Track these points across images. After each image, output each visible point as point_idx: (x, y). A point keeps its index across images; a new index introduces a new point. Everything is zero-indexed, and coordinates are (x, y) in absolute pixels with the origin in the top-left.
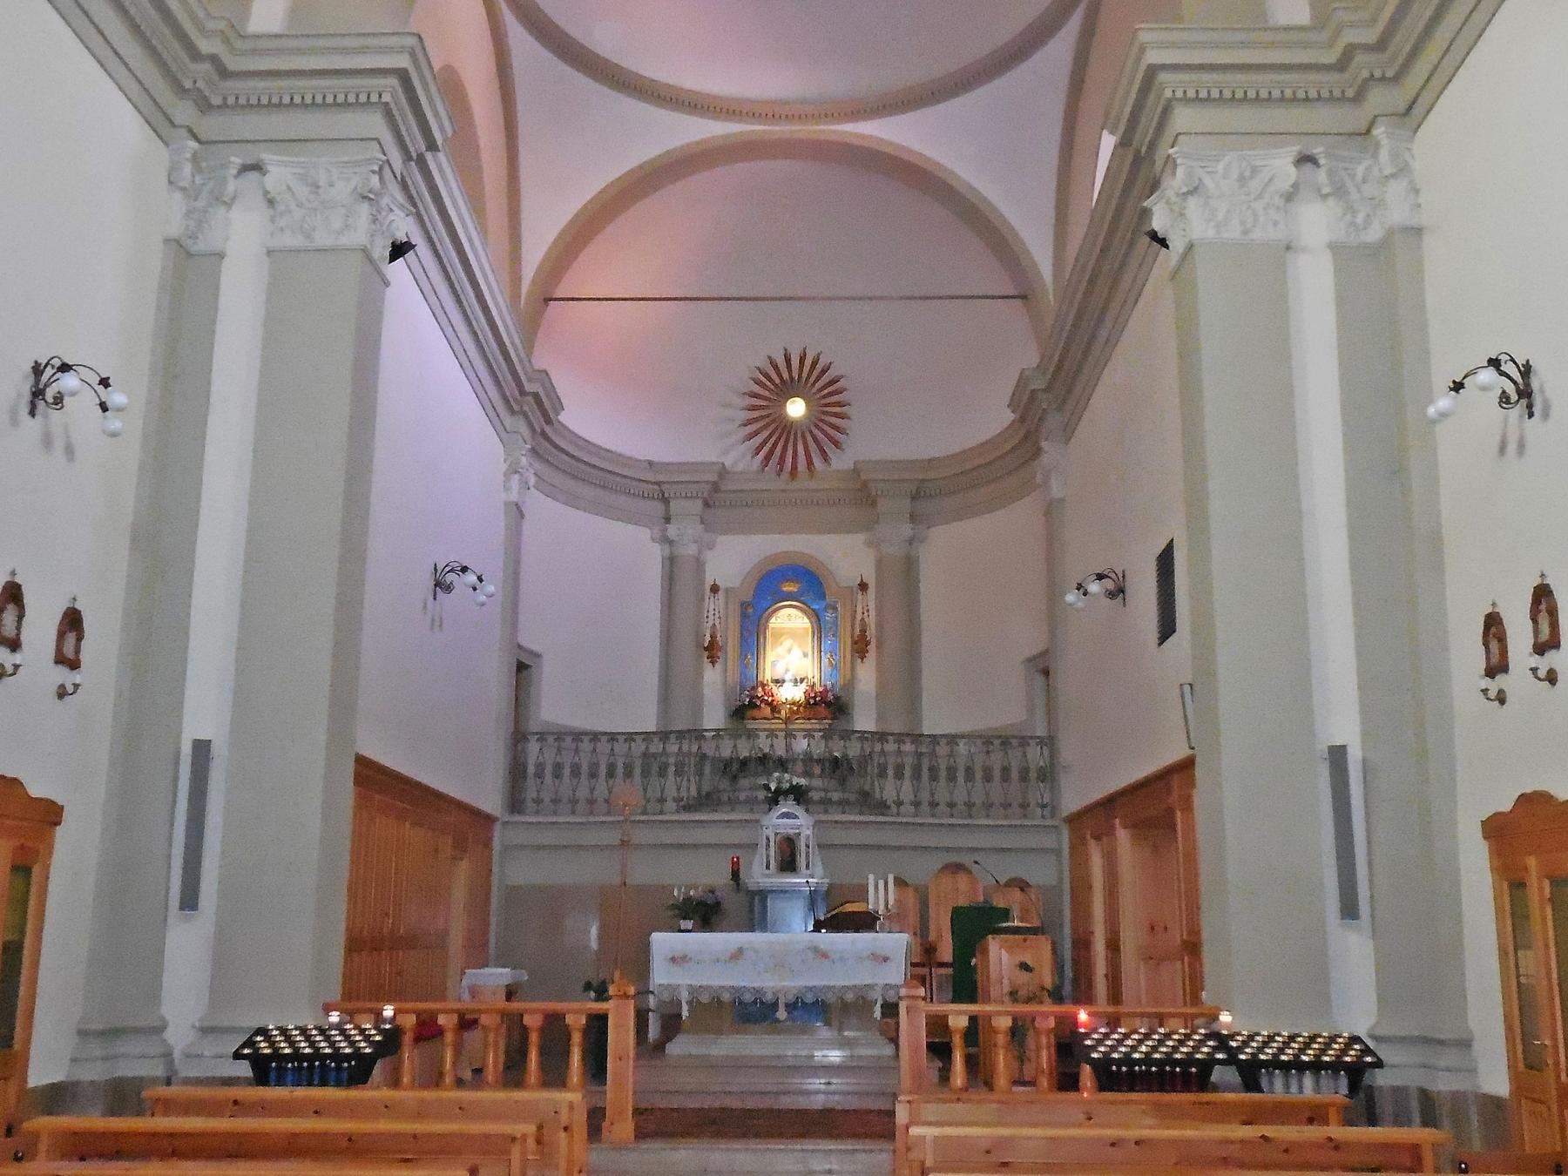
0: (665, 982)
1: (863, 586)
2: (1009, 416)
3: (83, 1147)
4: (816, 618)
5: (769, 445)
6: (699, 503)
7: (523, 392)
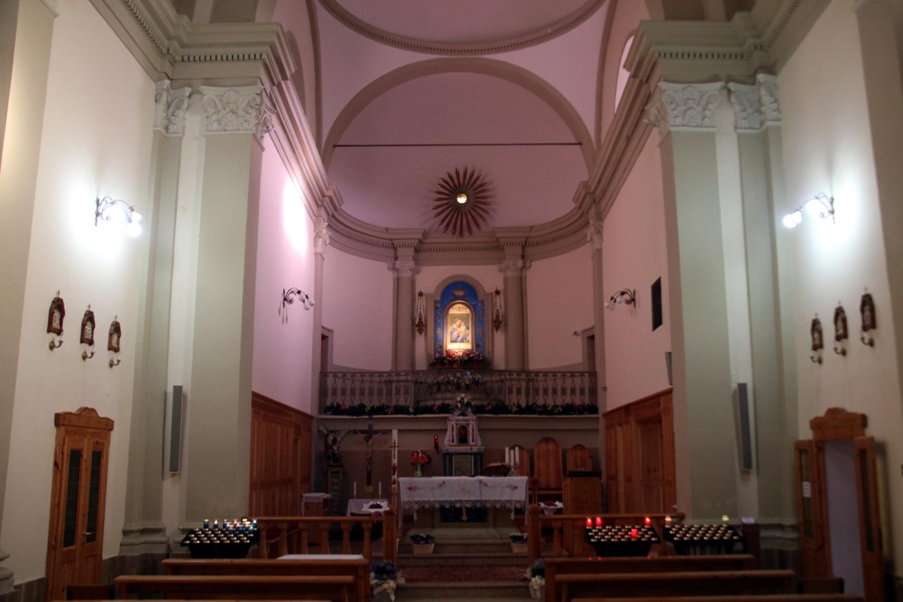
0: (406, 500)
1: (498, 293)
2: (572, 206)
3: (134, 589)
4: (473, 308)
5: (448, 220)
6: (412, 250)
7: (323, 196)
